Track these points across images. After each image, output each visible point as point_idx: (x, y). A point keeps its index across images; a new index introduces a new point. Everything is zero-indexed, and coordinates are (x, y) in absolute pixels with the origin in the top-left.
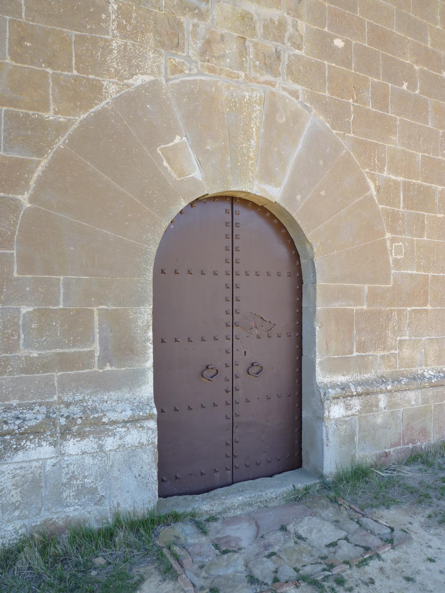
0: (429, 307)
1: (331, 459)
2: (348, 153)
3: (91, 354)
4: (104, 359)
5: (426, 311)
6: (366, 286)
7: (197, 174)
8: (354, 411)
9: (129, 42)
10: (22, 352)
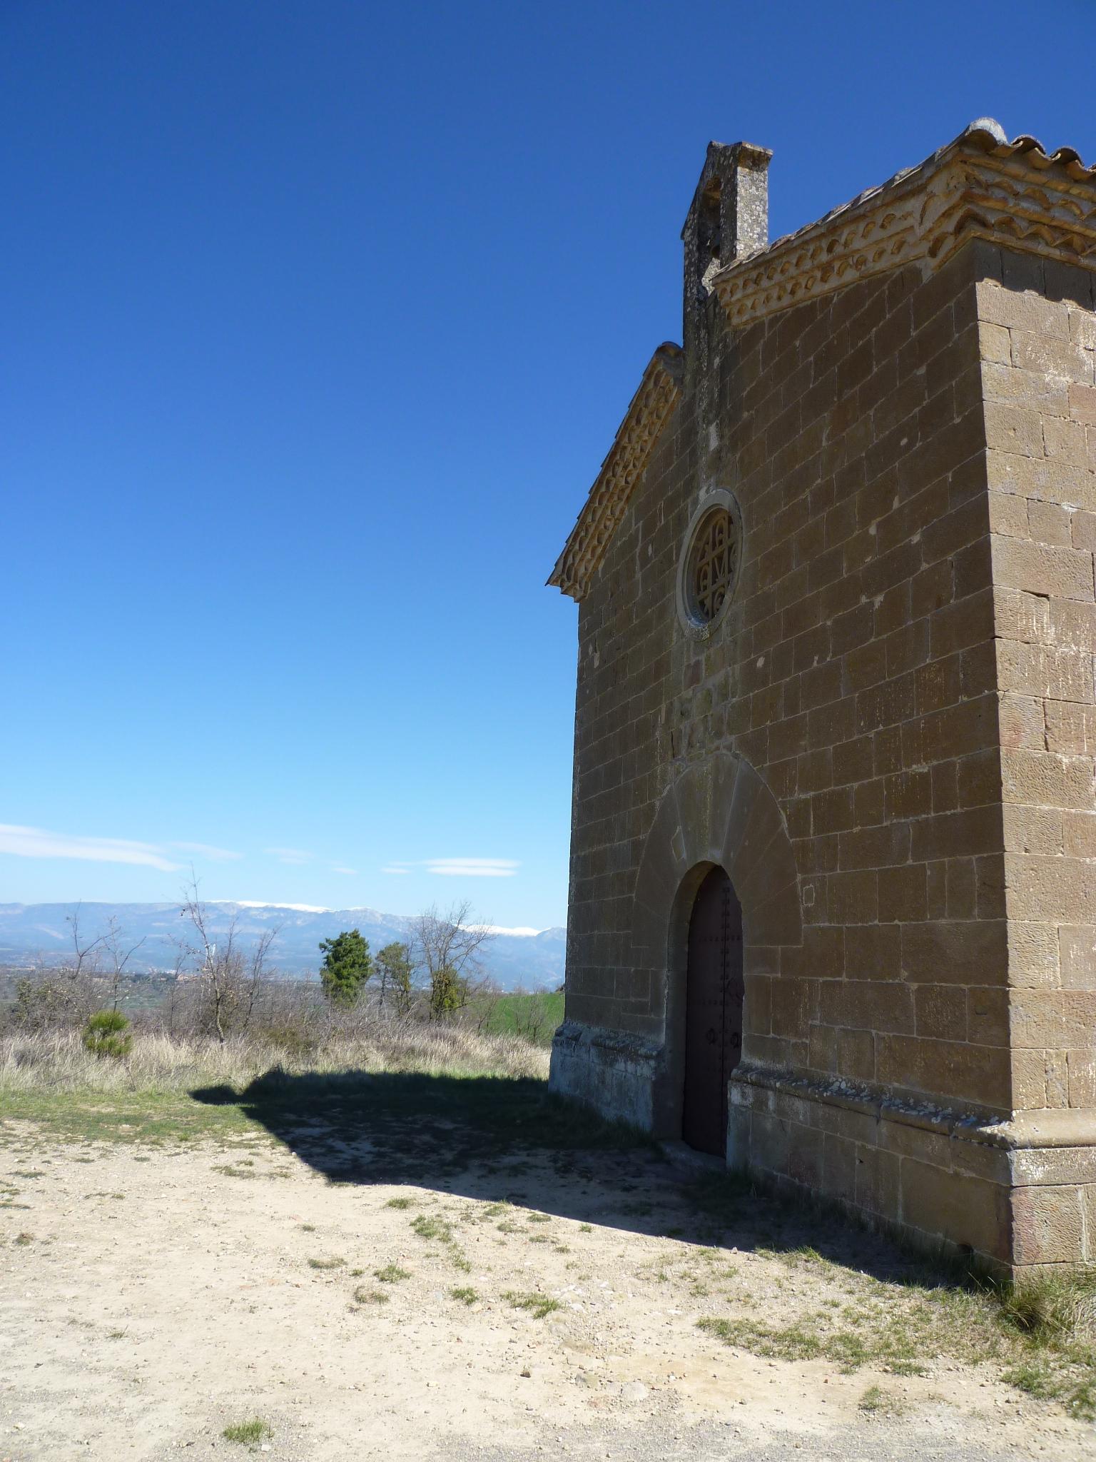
5: (840, 983)
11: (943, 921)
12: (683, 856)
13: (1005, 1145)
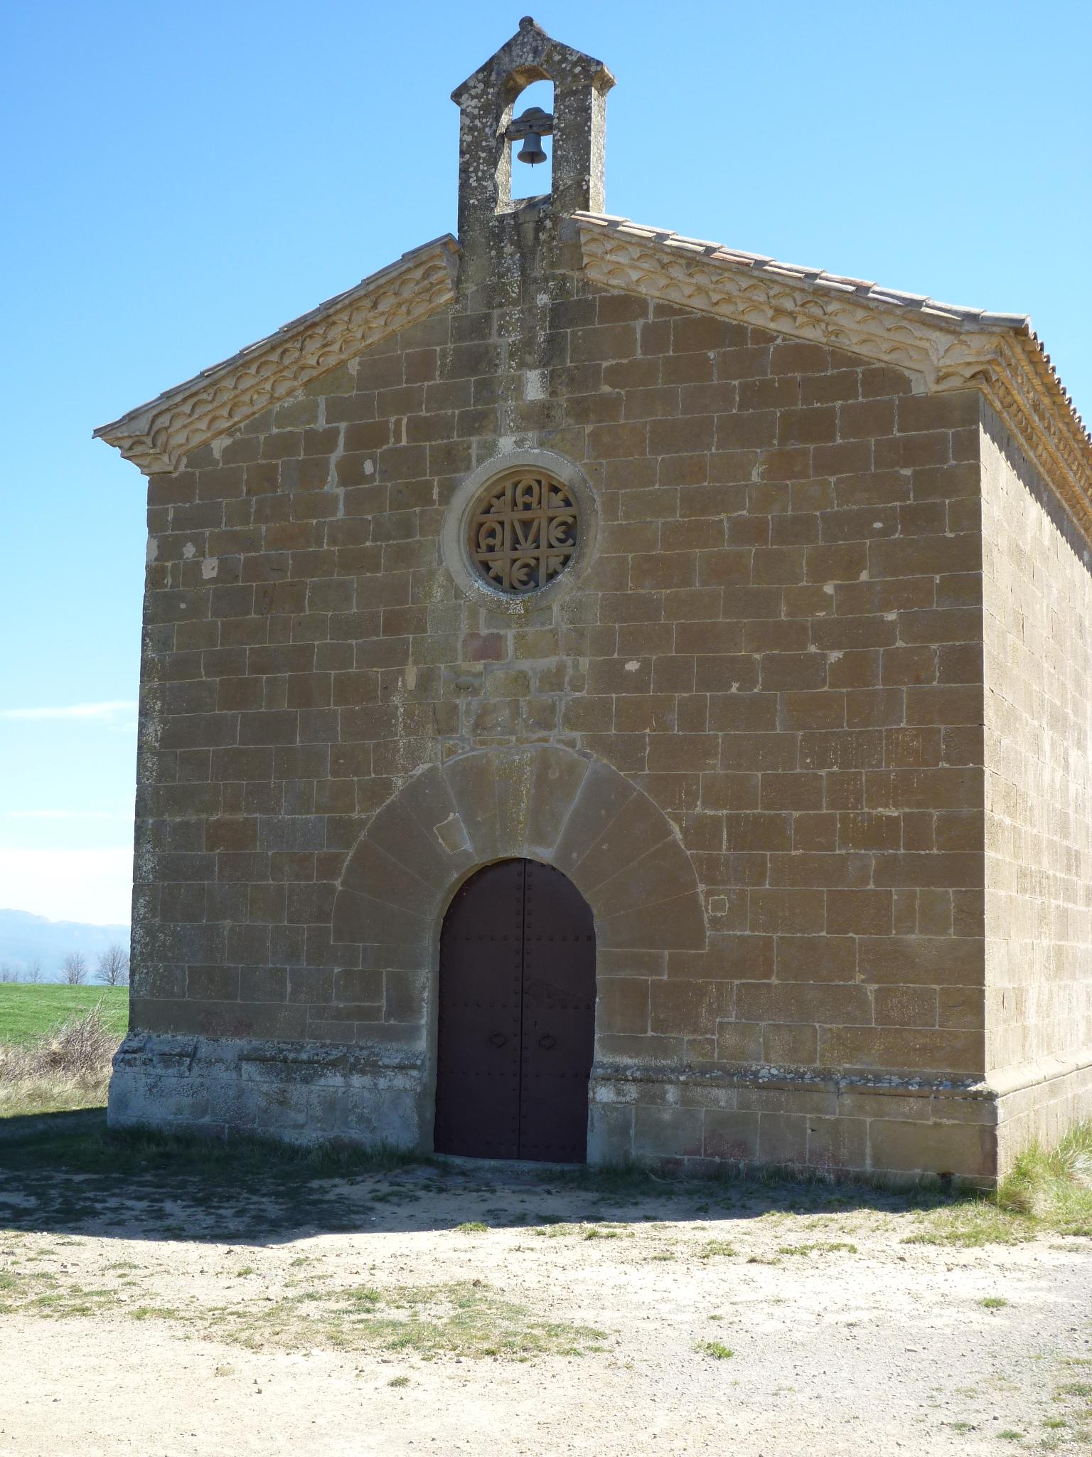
0: (774, 981)
1: (597, 1148)
2: (641, 794)
3: (379, 1008)
4: (389, 1014)
5: (769, 985)
6: (666, 952)
7: (468, 846)
8: (628, 1098)
9: (412, 738)
10: (334, 1003)
11: (913, 937)
12: (463, 845)
13: (991, 1096)
